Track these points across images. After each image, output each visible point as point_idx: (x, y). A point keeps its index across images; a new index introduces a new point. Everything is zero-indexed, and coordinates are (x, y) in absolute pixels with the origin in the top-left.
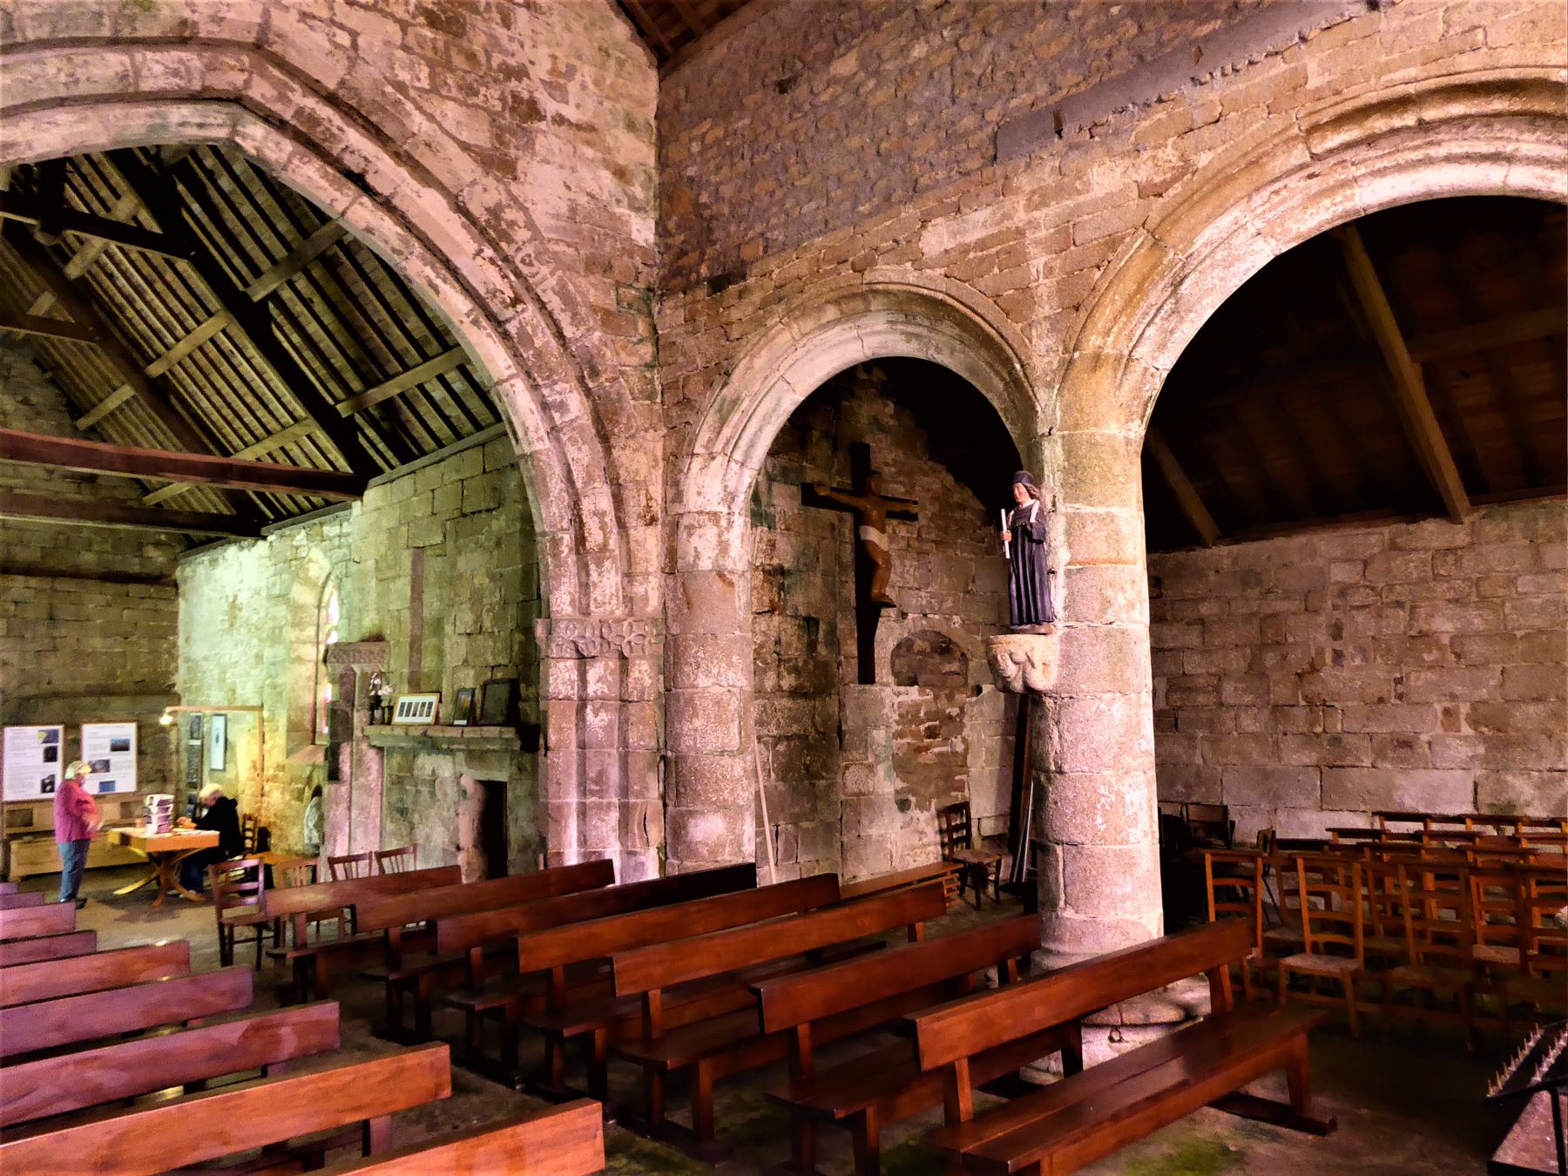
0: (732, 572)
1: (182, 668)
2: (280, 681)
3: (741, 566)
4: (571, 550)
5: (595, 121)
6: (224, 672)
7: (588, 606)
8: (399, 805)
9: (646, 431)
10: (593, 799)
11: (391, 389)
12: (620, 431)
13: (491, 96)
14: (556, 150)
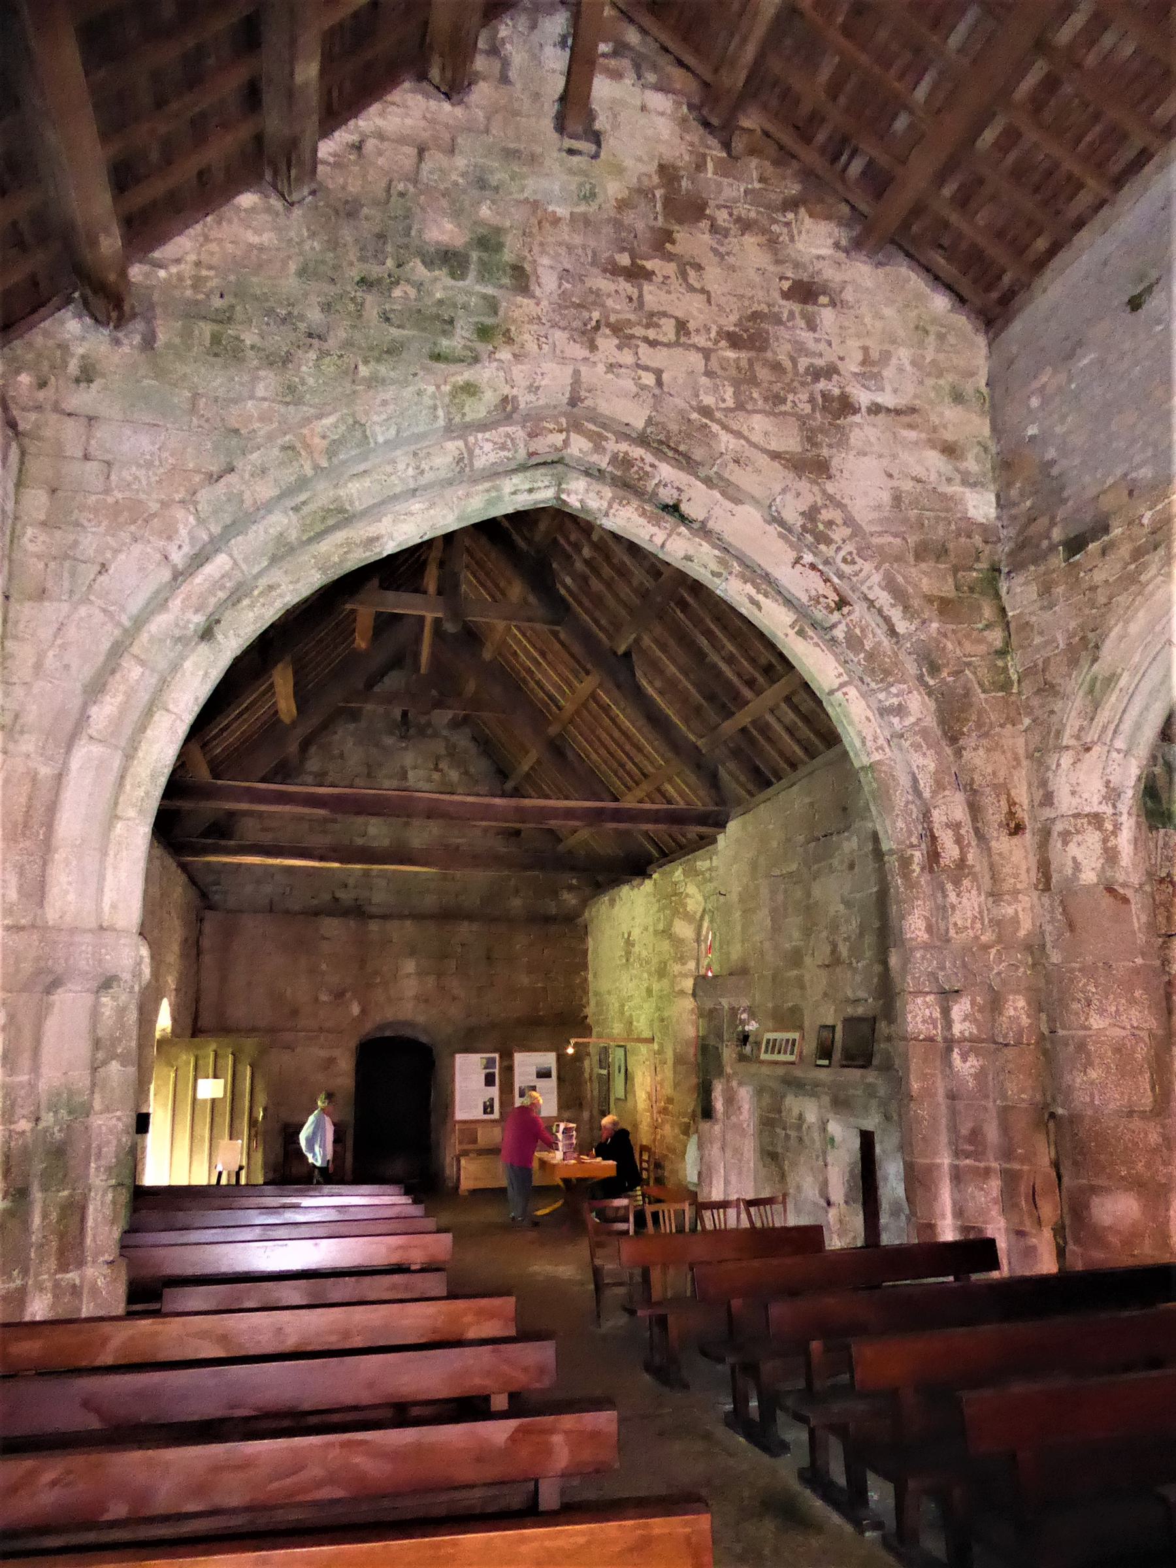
0: (1125, 885)
1: (592, 1002)
2: (666, 1014)
3: (1135, 880)
4: (923, 869)
5: (917, 402)
6: (623, 1006)
7: (947, 930)
8: (770, 1148)
9: (1002, 726)
10: (968, 1161)
11: (743, 718)
12: (970, 730)
13: (800, 401)
14: (873, 439)
